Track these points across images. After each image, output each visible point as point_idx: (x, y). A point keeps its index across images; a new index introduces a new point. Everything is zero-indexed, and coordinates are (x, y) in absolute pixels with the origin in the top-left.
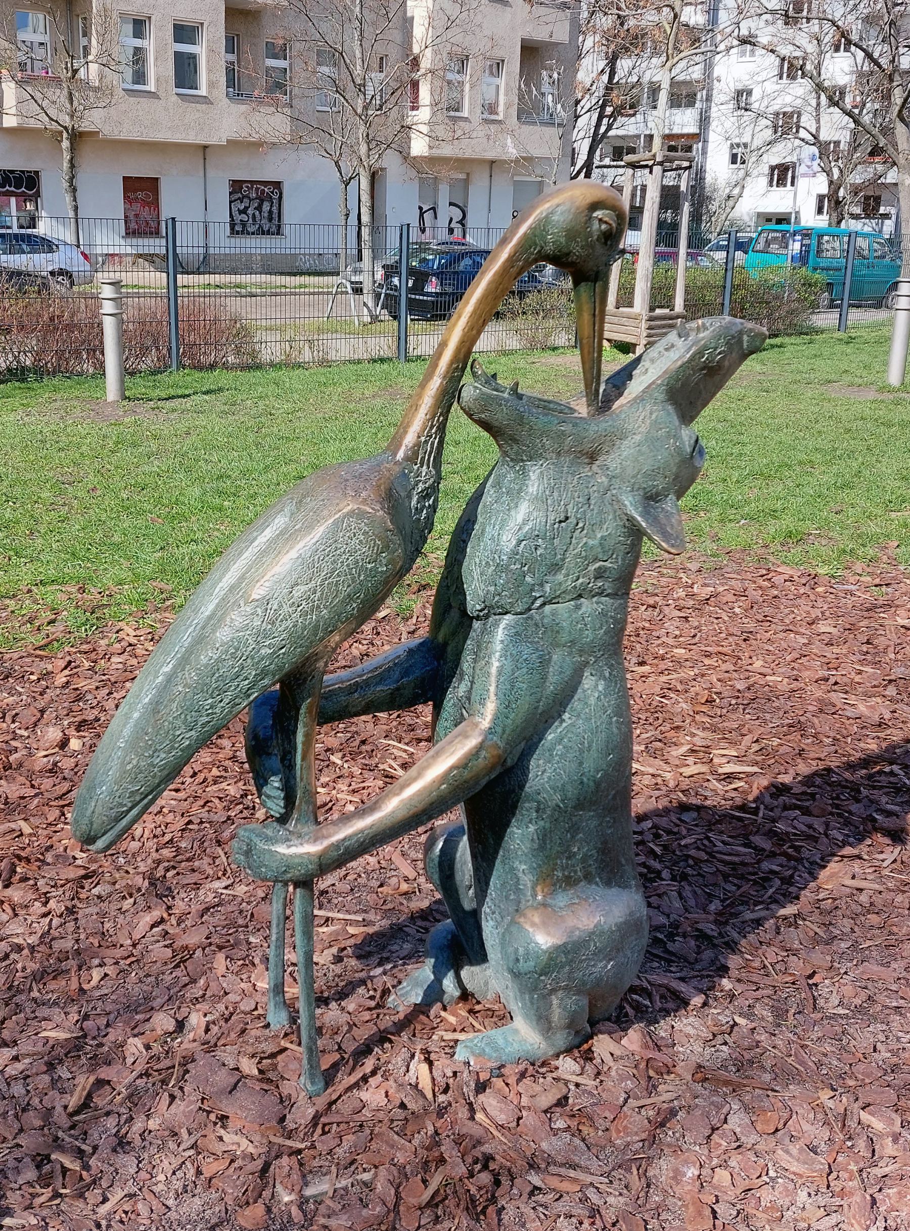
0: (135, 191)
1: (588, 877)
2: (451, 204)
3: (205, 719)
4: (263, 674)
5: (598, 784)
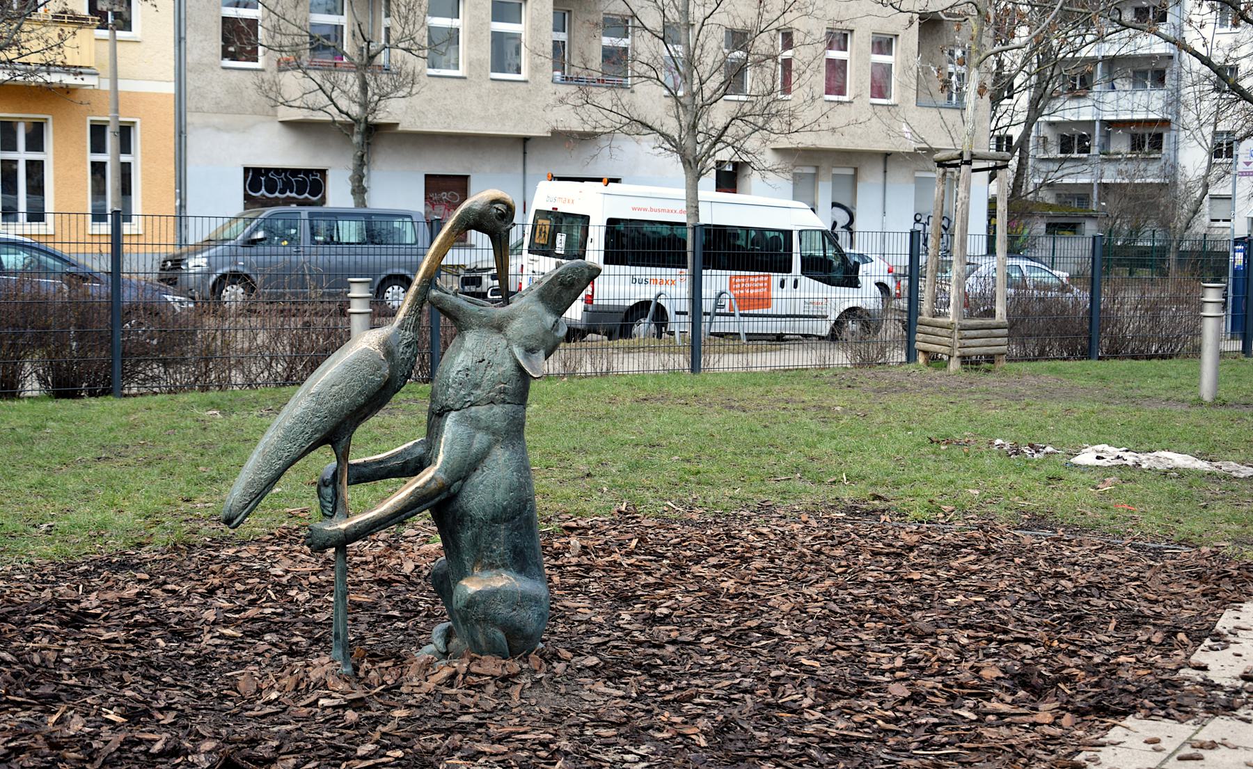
0: (439, 191)
1: (505, 566)
2: (834, 205)
4: (316, 431)
5: (505, 508)
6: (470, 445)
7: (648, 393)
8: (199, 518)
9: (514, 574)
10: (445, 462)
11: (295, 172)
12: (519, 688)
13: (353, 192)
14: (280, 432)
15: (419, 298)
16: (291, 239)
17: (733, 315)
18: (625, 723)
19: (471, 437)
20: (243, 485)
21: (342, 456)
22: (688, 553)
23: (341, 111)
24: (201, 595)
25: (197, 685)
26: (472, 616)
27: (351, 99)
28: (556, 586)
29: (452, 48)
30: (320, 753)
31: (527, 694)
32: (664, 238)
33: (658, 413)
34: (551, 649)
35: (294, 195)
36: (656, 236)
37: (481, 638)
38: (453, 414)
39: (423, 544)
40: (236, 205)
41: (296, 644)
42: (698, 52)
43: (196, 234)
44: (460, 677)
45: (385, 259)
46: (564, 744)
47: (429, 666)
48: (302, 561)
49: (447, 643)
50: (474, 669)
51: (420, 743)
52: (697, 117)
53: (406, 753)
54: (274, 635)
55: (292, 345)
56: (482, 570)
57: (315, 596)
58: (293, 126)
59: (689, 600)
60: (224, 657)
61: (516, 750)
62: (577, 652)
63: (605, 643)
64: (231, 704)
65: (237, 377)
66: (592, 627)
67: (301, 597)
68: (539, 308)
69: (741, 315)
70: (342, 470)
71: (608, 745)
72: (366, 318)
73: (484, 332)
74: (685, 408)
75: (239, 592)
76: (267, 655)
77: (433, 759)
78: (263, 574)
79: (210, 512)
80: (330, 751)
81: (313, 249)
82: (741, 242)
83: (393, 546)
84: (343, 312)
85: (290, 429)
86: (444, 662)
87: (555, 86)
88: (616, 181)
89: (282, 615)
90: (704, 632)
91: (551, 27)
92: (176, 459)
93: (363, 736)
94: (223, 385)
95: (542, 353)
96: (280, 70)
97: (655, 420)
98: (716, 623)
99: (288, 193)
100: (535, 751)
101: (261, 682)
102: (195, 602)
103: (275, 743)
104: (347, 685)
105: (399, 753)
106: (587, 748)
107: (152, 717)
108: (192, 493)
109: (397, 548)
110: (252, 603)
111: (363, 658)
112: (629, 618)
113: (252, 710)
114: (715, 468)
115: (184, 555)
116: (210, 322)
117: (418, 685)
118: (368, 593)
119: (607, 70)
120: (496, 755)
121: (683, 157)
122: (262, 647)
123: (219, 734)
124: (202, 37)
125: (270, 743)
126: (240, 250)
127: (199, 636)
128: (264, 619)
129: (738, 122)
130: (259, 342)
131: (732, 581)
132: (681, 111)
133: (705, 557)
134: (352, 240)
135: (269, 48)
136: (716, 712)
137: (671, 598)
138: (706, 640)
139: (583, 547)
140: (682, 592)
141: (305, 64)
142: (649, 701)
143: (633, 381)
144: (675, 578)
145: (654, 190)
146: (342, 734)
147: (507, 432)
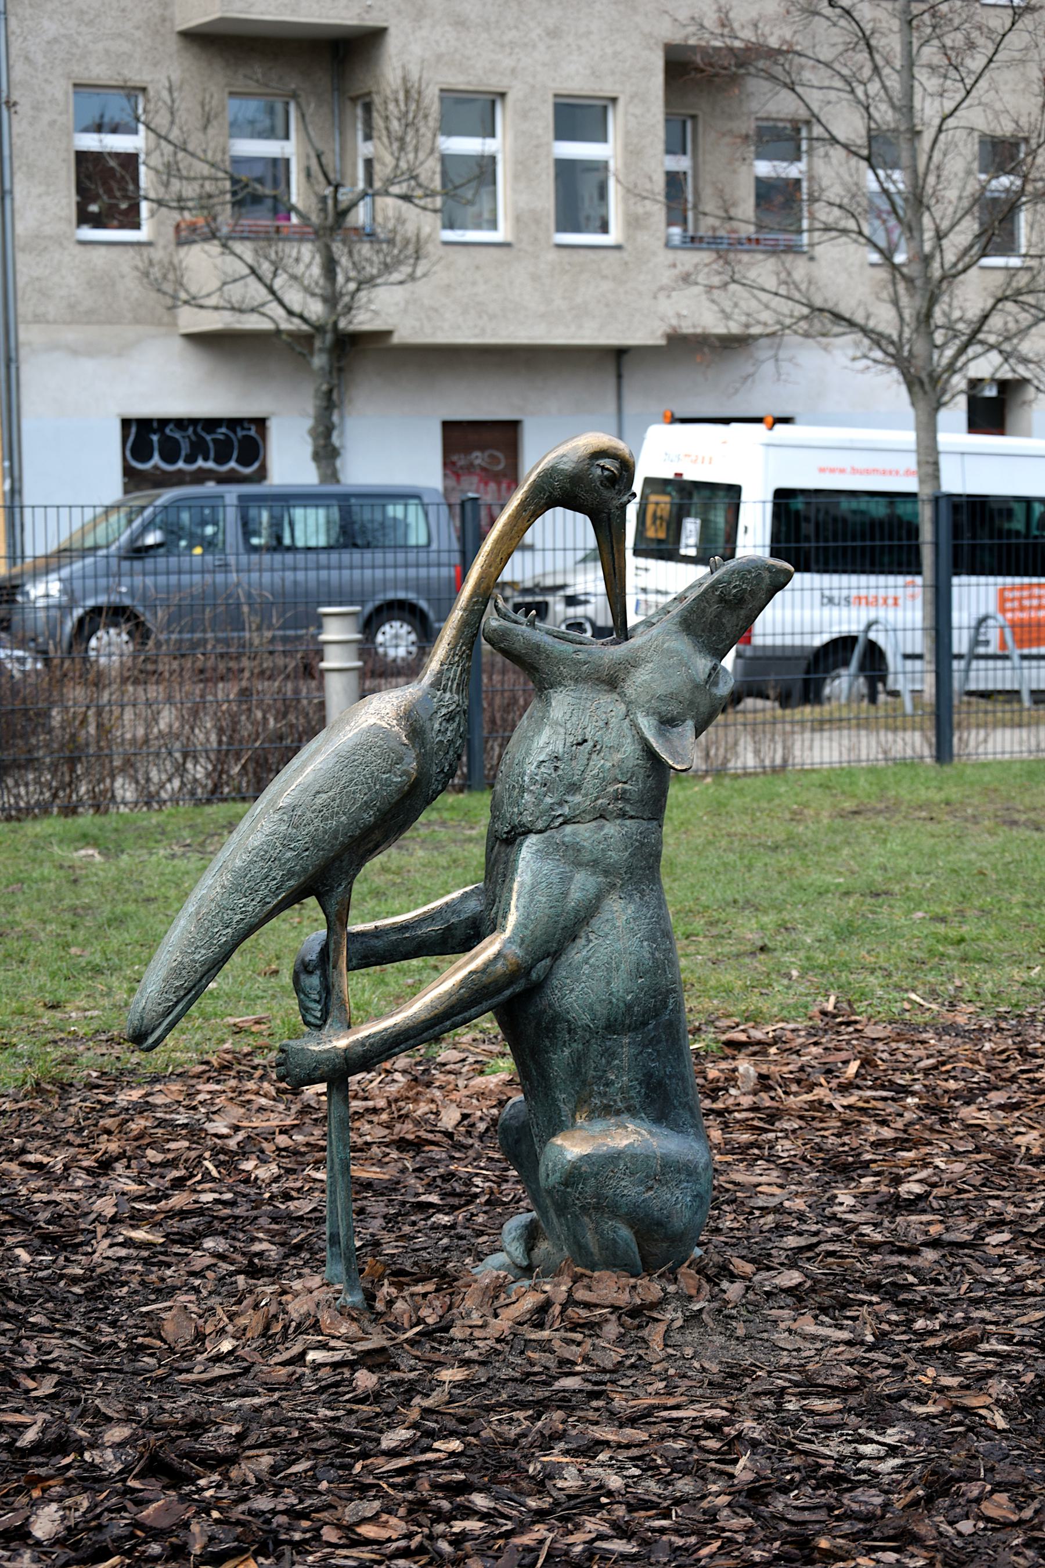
0: (468, 450)
1: (631, 1111)
3: (239, 917)
4: (291, 874)
5: (629, 1007)
6: (565, 894)
7: (864, 804)
8: (76, 1037)
9: (647, 1124)
10: (520, 926)
11: (211, 424)
12: (662, 1328)
13: (316, 457)
14: (227, 879)
15: (467, 631)
16: (209, 544)
17: (1005, 657)
18: (855, 1390)
19: (566, 879)
20: (163, 973)
21: (337, 920)
22: (952, 1085)
23: (290, 313)
24: (89, 1171)
25: (89, 1329)
26: (577, 1198)
27: (308, 291)
28: (717, 1146)
29: (485, 191)
30: (316, 1445)
31: (677, 1338)
32: (881, 523)
33: (881, 836)
34: (717, 1258)
35: (210, 465)
36: (858, 518)
37: (590, 1239)
38: (533, 838)
39: (481, 1070)
40: (110, 486)
41: (260, 1254)
42: (931, 180)
43: (39, 542)
44: (556, 1309)
45: (378, 573)
46: (748, 1425)
47: (499, 1288)
48: (261, 1109)
49: (529, 1249)
50: (581, 1295)
51: (491, 1427)
52: (933, 300)
53: (468, 1445)
54: (221, 1240)
55: (221, 731)
56: (590, 1118)
57: (289, 1171)
58: (202, 340)
59: (958, 1167)
60: (135, 1279)
61: (663, 1437)
62: (762, 1262)
63: (810, 1247)
64: (152, 1361)
65: (125, 789)
66: (786, 1219)
67: (264, 1173)
68: (682, 644)
69: (1024, 657)
70: (338, 944)
71: (828, 1428)
72: (353, 678)
73: (585, 691)
74: (930, 827)
75: (153, 1165)
76: (210, 1274)
77: (516, 1455)
78: (194, 1133)
79: (95, 1025)
80: (332, 1441)
81: (244, 559)
82: (1018, 525)
83: (420, 1081)
84: (310, 670)
85: (244, 873)
86: (526, 1283)
87: (671, 256)
88: (786, 420)
89: (232, 1204)
90: (990, 1225)
91: (661, 147)
92: (29, 934)
93: (388, 1414)
94: (101, 803)
95: (690, 724)
96: (180, 243)
97: (876, 849)
98: (1011, 1209)
99: (200, 463)
100: (697, 1439)
101: (202, 1321)
102: (79, 1183)
103: (235, 1429)
104: (354, 1327)
105: (455, 1445)
106: (791, 1434)
107: (15, 1384)
108: (61, 994)
109: (429, 1085)
110: (178, 1184)
111: (381, 1277)
112: (849, 1201)
113: (189, 1371)
114: (991, 932)
115: (55, 1102)
116: (76, 693)
117: (482, 1326)
118: (381, 1163)
119: (769, 220)
120: (628, 1447)
121: (905, 374)
122: (200, 1260)
123: (135, 1413)
124: (42, 189)
125: (226, 1429)
126: (126, 565)
127: (88, 1243)
128: (200, 1211)
129: (1009, 306)
130: (163, 725)
131: (1035, 1134)
132: (901, 287)
133: (984, 1092)
134: (312, 543)
135: (160, 203)
136: (1020, 1367)
137: (926, 1165)
138: (995, 1238)
139: (762, 1077)
140: (945, 1154)
141: (225, 230)
142: (896, 1348)
143: (829, 781)
144: (932, 1130)
145: (858, 438)
146: (351, 1412)
147: (630, 870)
